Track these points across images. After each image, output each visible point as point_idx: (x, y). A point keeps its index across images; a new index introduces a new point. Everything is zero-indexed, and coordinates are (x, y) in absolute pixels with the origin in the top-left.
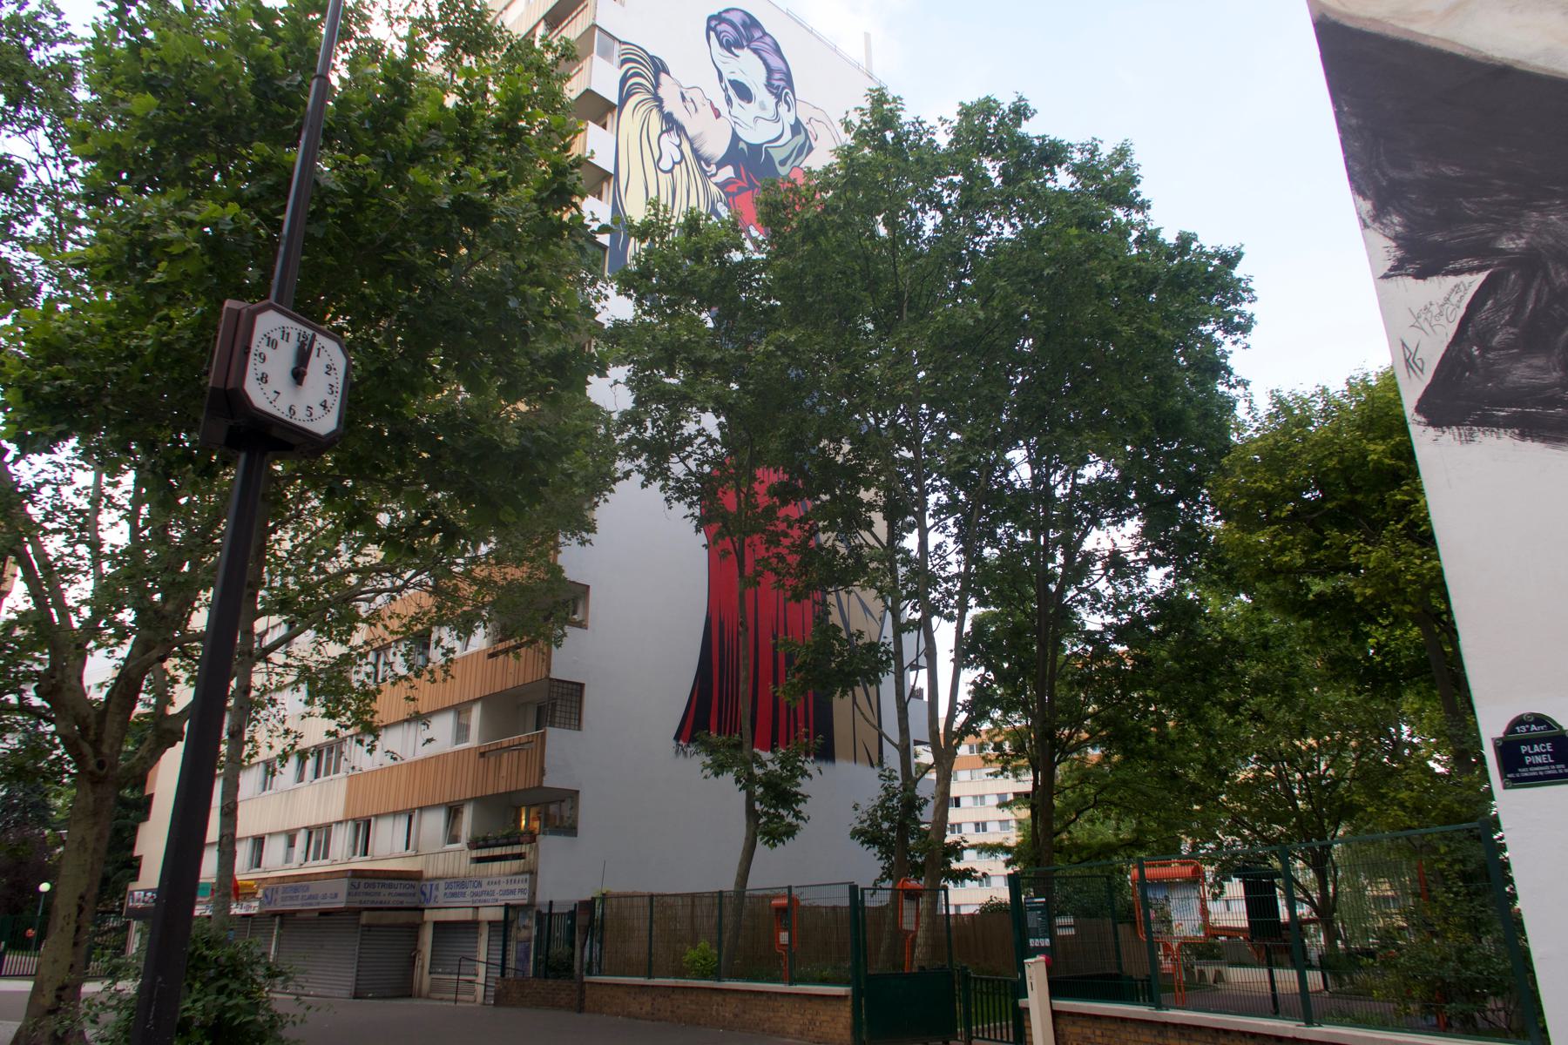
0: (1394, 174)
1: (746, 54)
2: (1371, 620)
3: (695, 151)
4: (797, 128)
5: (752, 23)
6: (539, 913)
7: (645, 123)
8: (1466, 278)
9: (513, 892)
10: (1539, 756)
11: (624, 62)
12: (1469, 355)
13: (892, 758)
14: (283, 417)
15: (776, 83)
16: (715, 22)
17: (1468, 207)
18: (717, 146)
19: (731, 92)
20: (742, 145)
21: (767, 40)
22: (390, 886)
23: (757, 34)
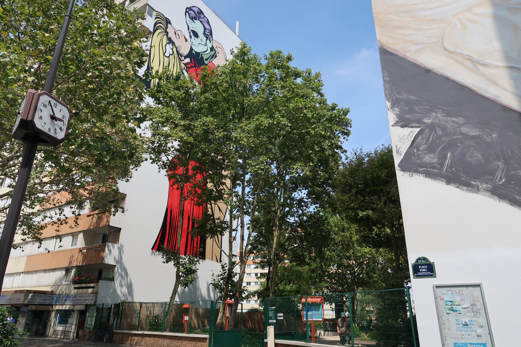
0: (397, 96)
1: (197, 22)
2: (375, 225)
3: (177, 51)
4: (212, 49)
5: (201, 12)
6: (97, 308)
7: (161, 40)
8: (414, 129)
9: (46, 300)
10: (423, 269)
11: (156, 18)
12: (414, 152)
13: (225, 260)
14: (46, 132)
15: (207, 33)
16: (189, 10)
17: (417, 108)
18: (185, 51)
19: (192, 34)
20: (193, 52)
21: (205, 18)
22: (41, 296)
23: (202, 16)
